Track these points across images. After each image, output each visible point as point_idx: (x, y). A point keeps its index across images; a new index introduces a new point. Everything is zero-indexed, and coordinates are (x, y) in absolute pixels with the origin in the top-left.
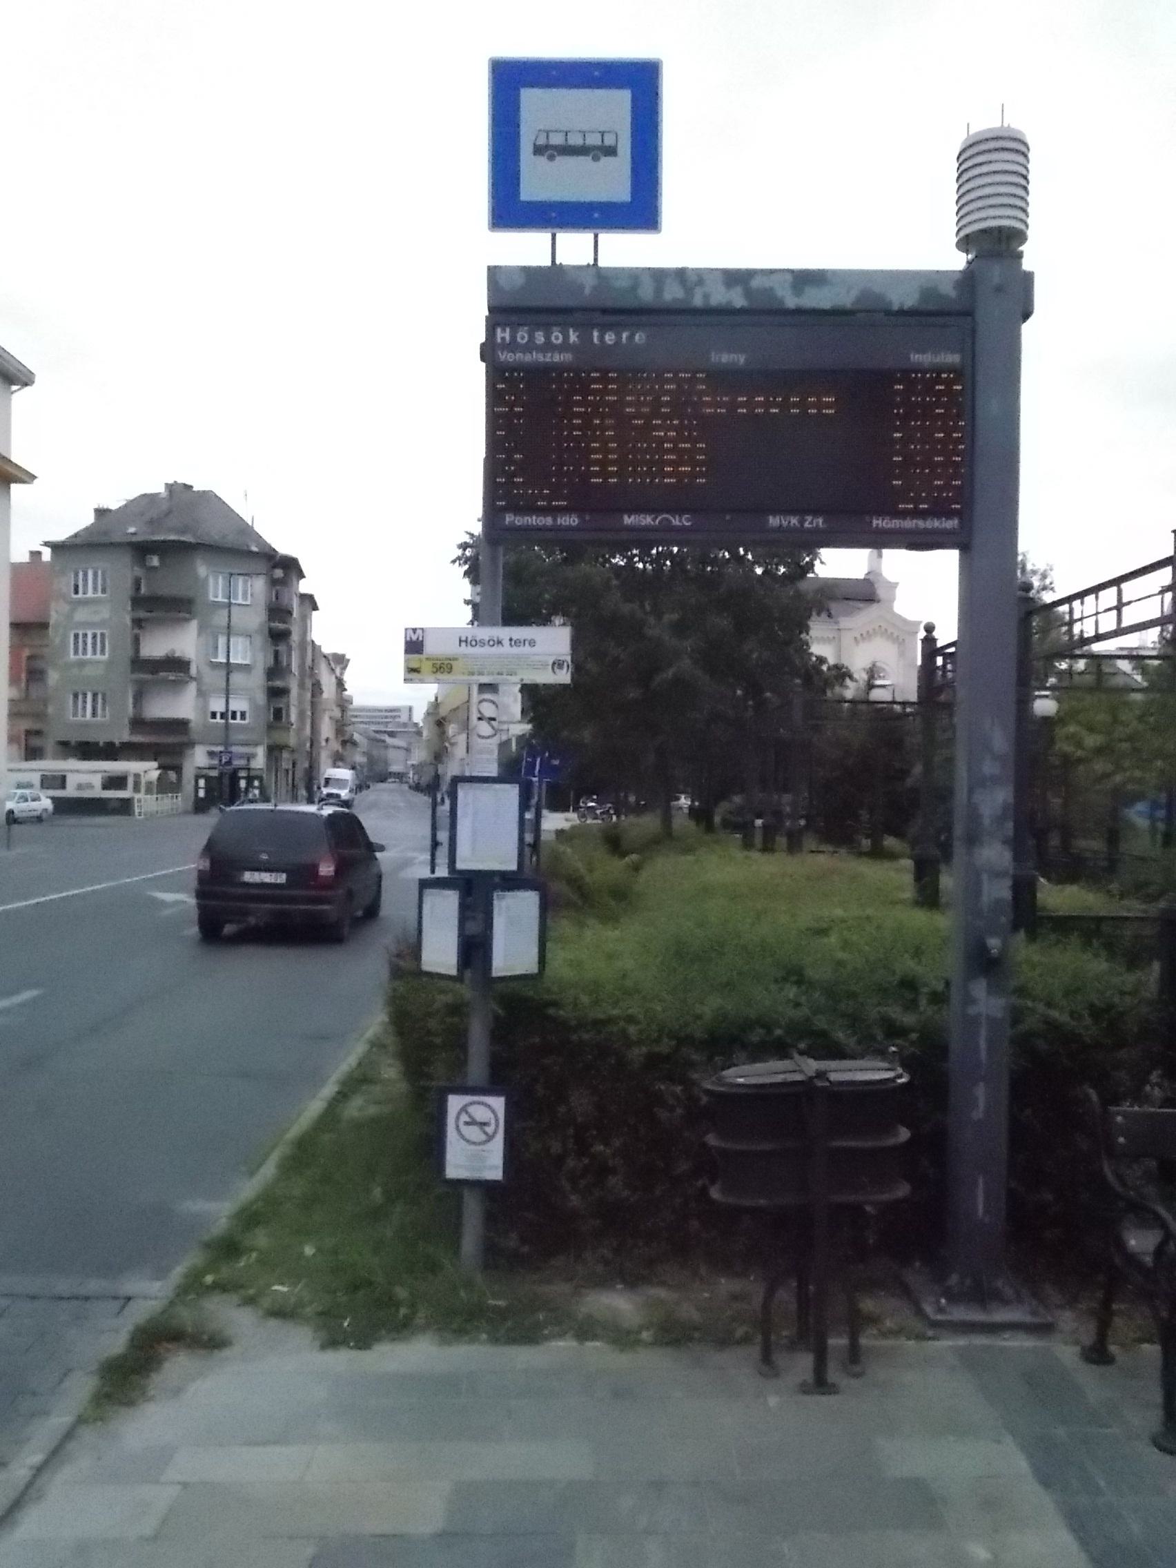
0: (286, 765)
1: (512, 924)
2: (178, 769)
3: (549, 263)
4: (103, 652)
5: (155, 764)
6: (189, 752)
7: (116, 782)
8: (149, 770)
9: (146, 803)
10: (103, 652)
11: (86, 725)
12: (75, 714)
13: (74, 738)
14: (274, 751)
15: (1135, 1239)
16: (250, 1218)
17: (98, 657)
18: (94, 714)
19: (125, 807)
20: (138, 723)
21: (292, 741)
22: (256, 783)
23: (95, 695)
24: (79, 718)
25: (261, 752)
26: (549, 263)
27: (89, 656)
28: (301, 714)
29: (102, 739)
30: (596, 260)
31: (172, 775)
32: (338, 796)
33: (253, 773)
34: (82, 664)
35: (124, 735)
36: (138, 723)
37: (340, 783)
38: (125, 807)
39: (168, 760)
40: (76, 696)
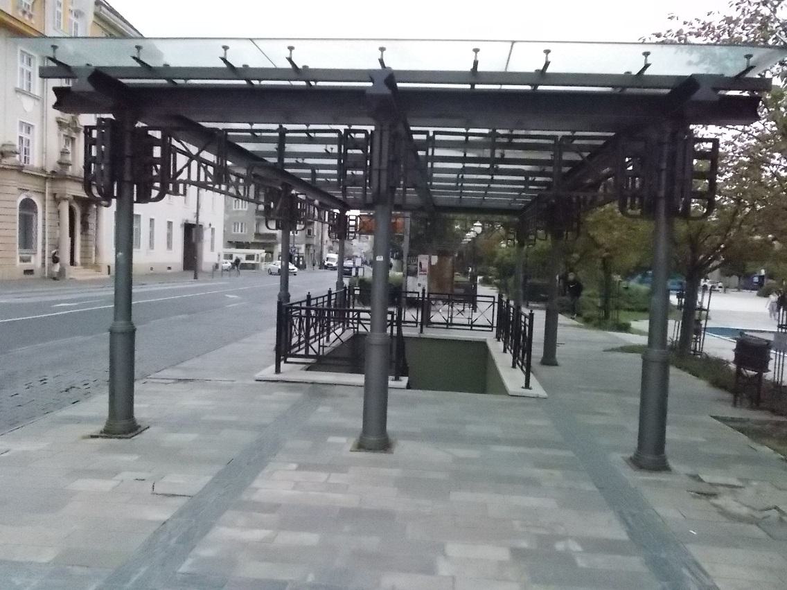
0: (311, 251)
1: (778, 215)
2: (272, 253)
3: (478, 294)
4: (245, 207)
5: (264, 251)
6: (276, 246)
7: (250, 257)
8: (261, 253)
9: (264, 266)
10: (245, 207)
11: (238, 235)
12: (235, 231)
13: (234, 240)
14: (308, 246)
15: (439, 256)
16: (602, 205)
17: (244, 209)
18: (242, 231)
19: (254, 267)
20: (258, 235)
21: (315, 243)
22: (301, 259)
23: (242, 224)
24: (236, 233)
25: (303, 247)
26: (478, 294)
27: (240, 209)
28: (318, 232)
29: (244, 241)
30: (479, 296)
31: (270, 255)
32: (332, 265)
33: (300, 255)
34: (237, 212)
35: (252, 239)
36: (258, 235)
37: (333, 260)
38: (254, 267)
39: (268, 249)
40: (235, 223)
